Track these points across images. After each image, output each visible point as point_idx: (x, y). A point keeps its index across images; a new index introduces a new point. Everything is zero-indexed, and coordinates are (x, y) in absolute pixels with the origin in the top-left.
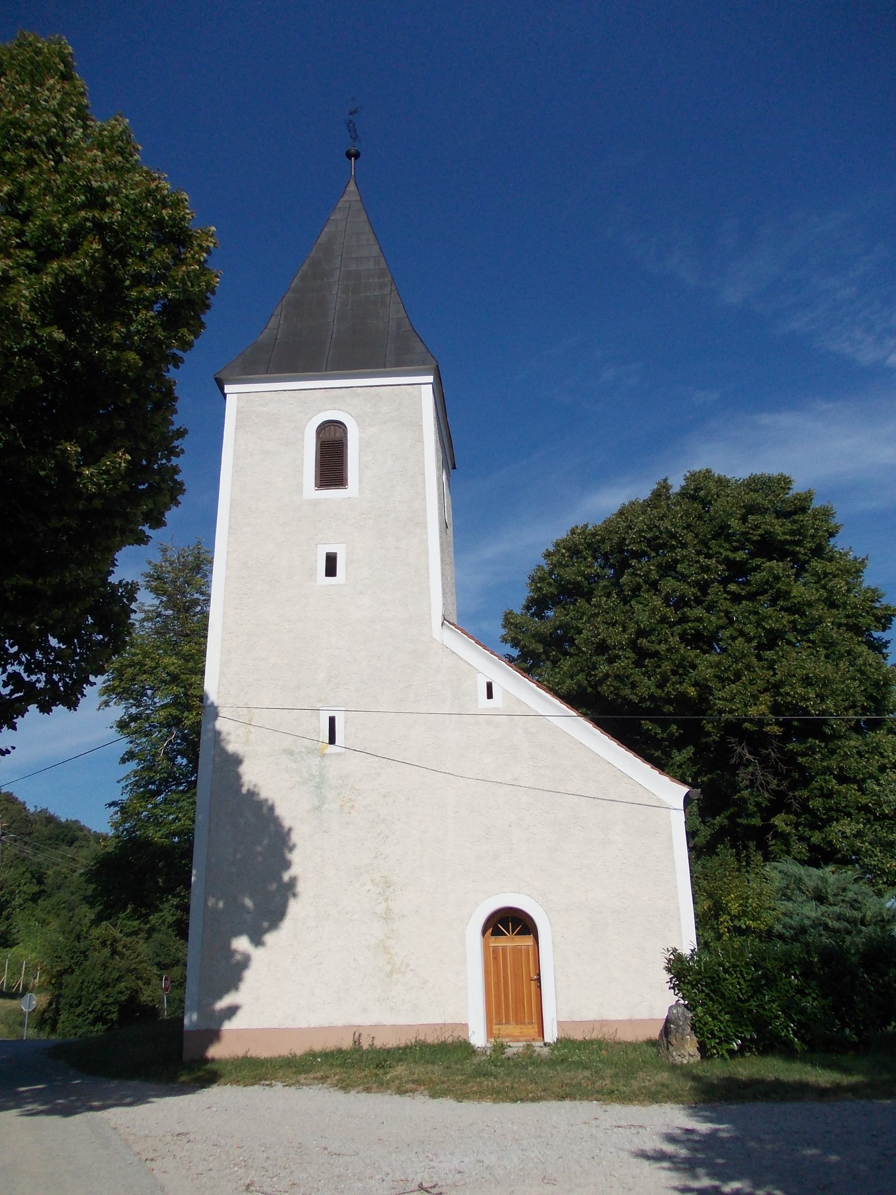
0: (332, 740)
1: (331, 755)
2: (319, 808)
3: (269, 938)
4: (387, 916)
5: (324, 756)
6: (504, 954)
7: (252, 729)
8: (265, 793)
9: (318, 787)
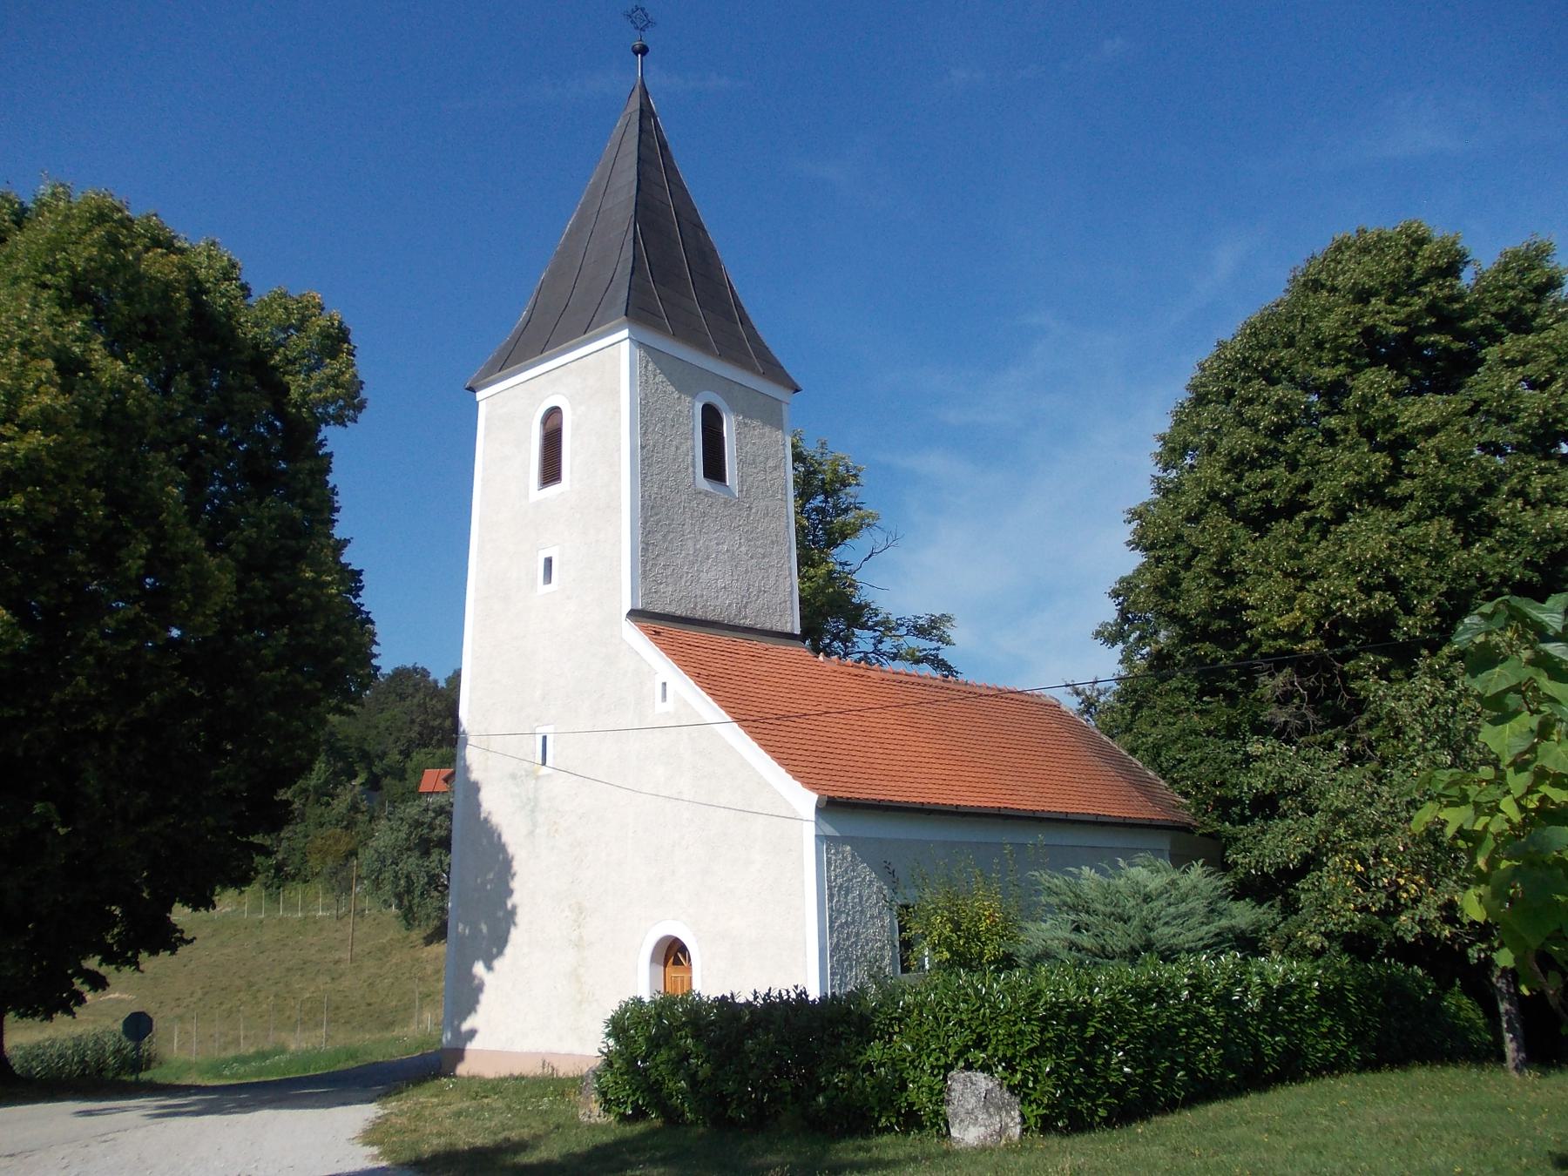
0: (544, 763)
1: (544, 776)
2: (531, 833)
3: (497, 964)
4: (579, 945)
5: (537, 778)
6: (682, 981)
7: (489, 754)
8: (495, 819)
9: (533, 811)
